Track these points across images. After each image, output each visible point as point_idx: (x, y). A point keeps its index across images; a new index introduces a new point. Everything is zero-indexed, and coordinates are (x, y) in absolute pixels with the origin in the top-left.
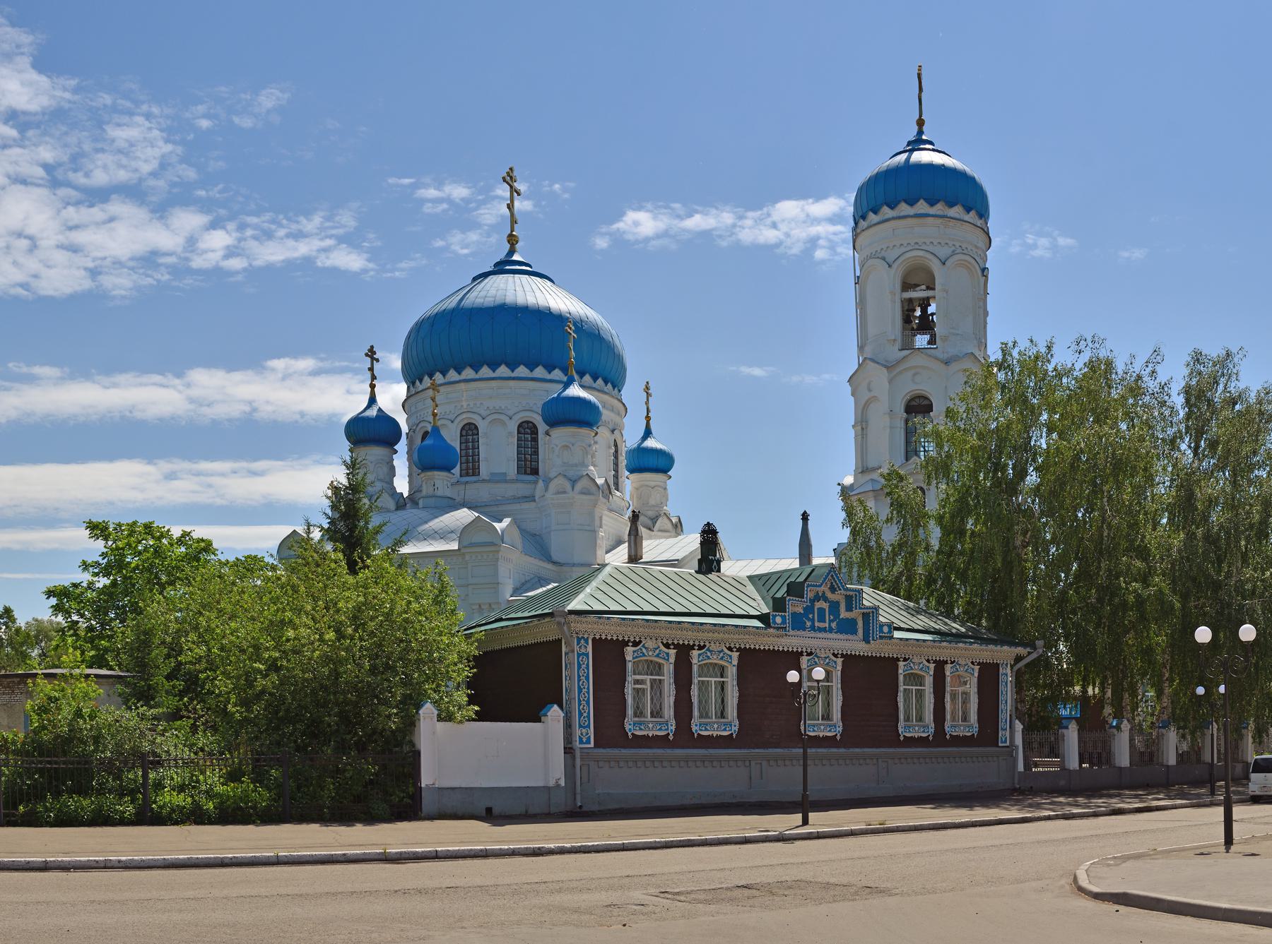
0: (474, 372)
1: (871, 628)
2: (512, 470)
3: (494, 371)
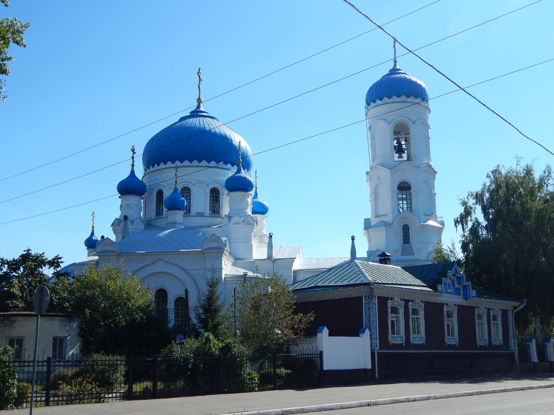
0: (190, 163)
1: (468, 291)
2: (208, 212)
3: (209, 164)
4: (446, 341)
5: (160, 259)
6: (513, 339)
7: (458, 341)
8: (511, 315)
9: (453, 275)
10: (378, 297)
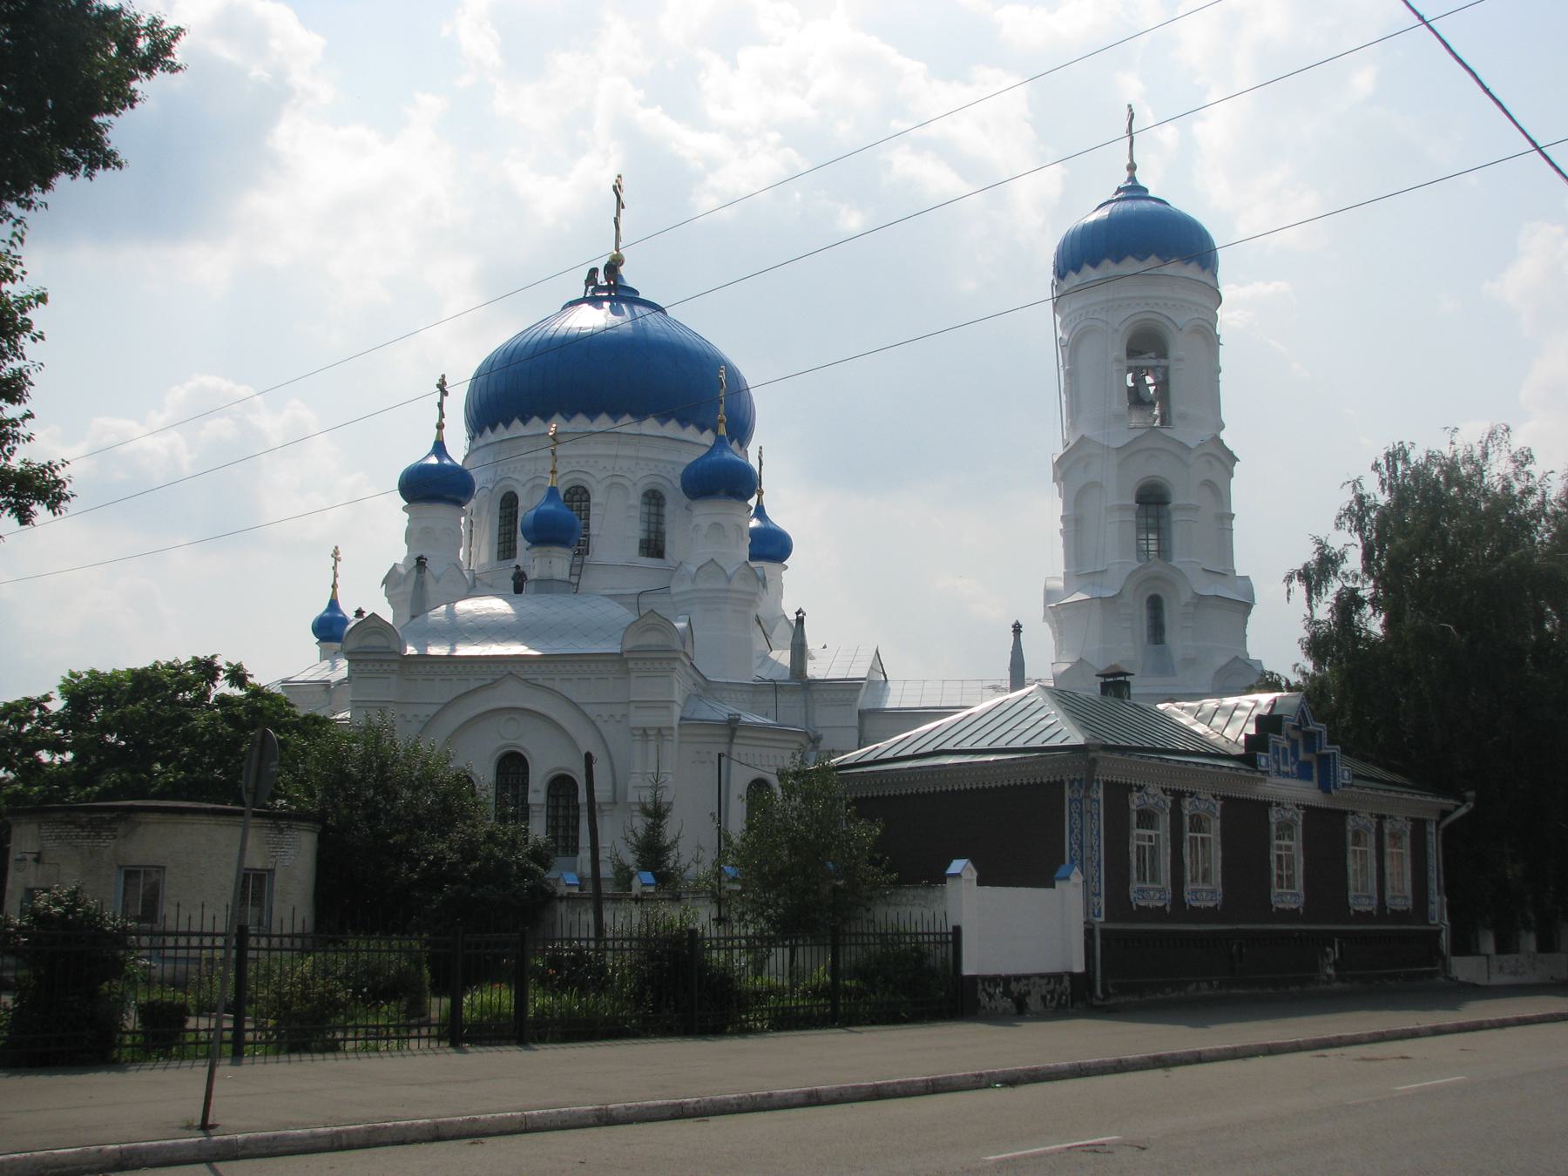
4: (1273, 899)
5: (510, 673)
6: (1439, 893)
7: (1302, 900)
8: (1434, 831)
9: (1294, 728)
10: (1106, 783)
